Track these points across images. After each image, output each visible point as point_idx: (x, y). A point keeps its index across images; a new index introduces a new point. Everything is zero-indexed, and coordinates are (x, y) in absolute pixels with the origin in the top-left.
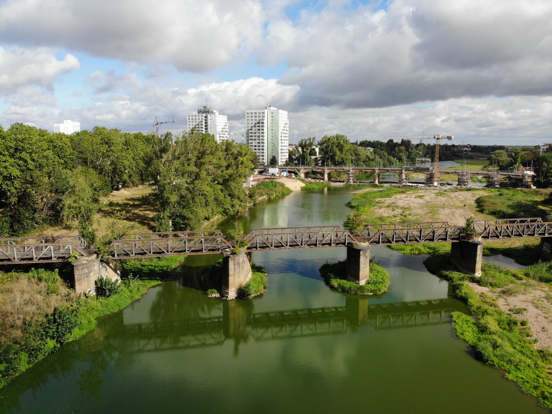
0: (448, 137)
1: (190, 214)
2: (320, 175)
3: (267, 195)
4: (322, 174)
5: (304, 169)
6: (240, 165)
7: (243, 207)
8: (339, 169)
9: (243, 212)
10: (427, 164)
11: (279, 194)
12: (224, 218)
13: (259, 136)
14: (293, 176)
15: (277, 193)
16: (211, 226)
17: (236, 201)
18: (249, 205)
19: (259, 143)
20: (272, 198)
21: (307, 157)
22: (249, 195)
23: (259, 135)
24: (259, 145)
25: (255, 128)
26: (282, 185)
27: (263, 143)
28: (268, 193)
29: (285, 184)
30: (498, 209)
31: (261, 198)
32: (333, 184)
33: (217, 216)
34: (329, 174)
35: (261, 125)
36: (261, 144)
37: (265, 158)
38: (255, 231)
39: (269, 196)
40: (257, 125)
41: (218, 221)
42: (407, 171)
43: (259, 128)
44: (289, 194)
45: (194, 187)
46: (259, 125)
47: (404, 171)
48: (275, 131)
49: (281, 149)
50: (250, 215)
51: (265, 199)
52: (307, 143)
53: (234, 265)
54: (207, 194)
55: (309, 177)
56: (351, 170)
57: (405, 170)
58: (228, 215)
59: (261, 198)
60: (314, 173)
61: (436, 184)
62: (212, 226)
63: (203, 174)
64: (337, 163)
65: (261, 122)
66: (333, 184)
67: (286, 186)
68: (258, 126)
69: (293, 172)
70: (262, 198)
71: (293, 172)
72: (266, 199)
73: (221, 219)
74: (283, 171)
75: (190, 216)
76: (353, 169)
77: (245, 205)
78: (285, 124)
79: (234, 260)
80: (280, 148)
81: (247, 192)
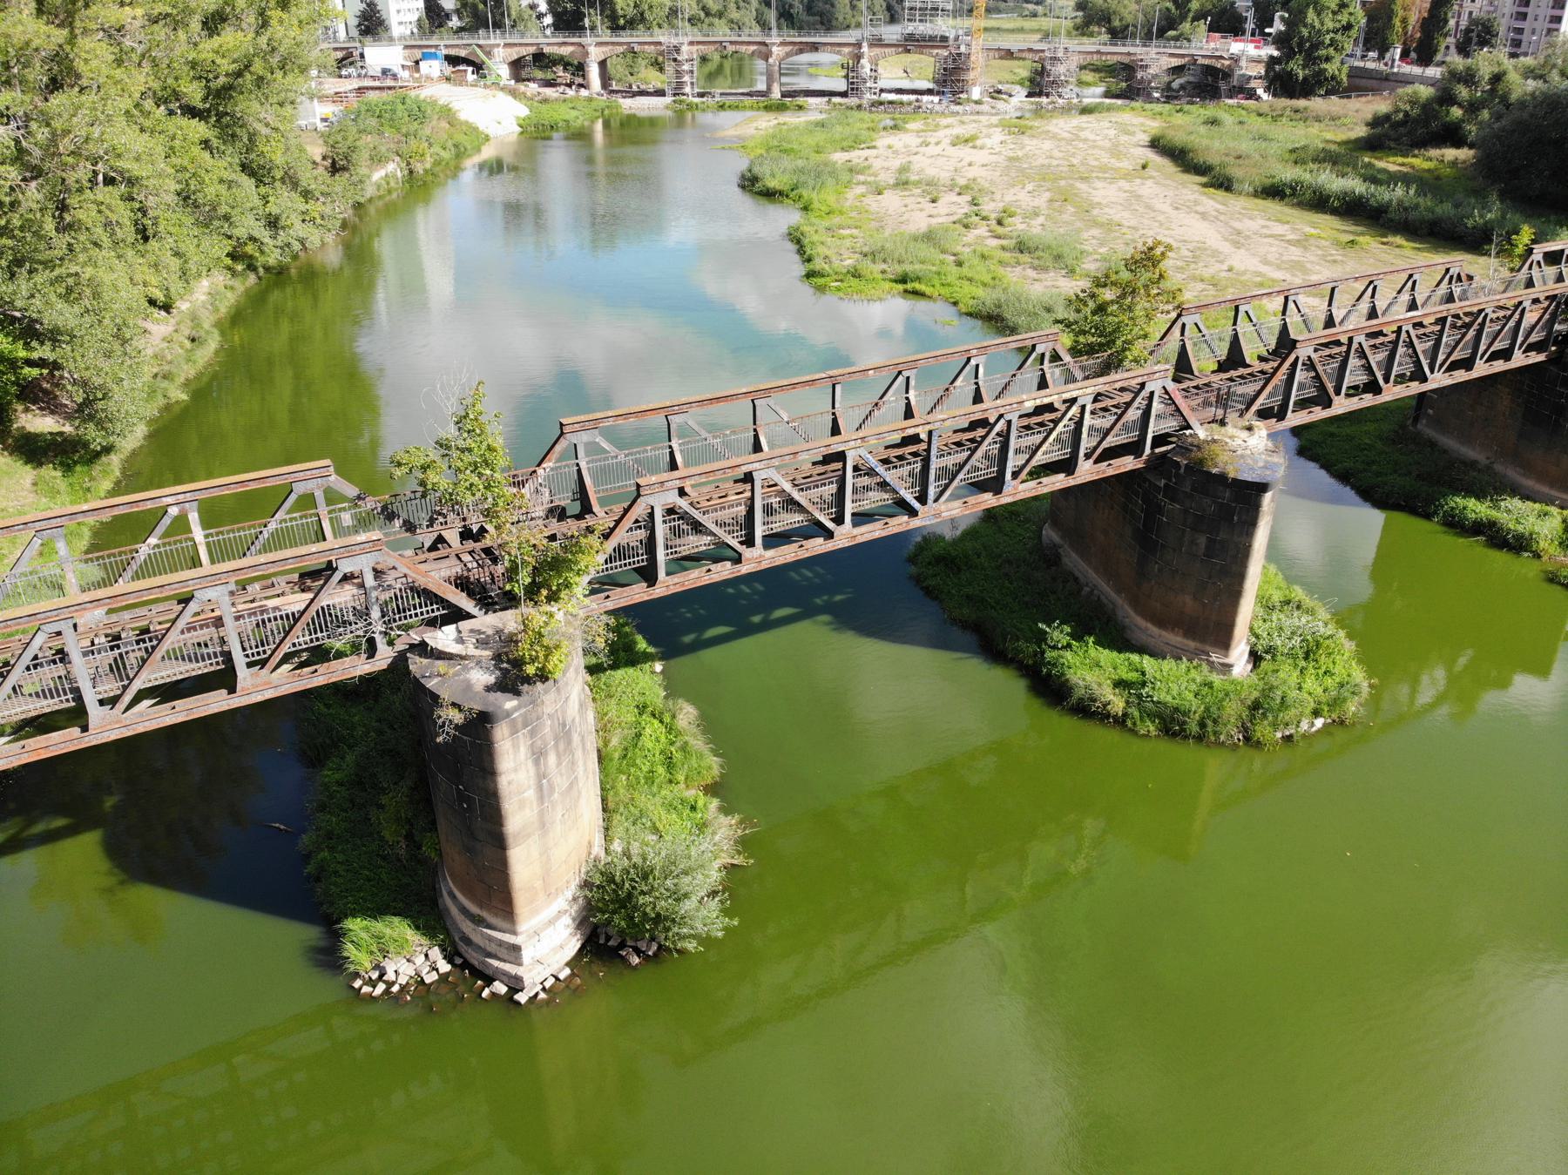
1: (60, 305)
2: (565, 69)
3: (397, 159)
5: (506, 45)
6: (279, 13)
7: (319, 221)
8: (639, 43)
10: (939, 21)
14: (471, 77)
15: (436, 149)
16: (188, 344)
17: (284, 201)
22: (328, 163)
26: (447, 114)
28: (404, 149)
29: (455, 106)
30: (1289, 179)
31: (377, 175)
32: (628, 105)
39: (408, 164)
41: (217, 310)
42: (876, 45)
45: (54, 134)
47: (865, 49)
53: (537, 762)
54: (136, 169)
55: (529, 80)
56: (685, 48)
57: (871, 45)
59: (377, 175)
60: (540, 59)
61: (976, 93)
63: (93, 55)
64: (622, 22)
66: (628, 105)
67: (462, 116)
70: (382, 173)
73: (229, 294)
74: (425, 57)
75: (58, 314)
76: (691, 43)
79: (531, 724)
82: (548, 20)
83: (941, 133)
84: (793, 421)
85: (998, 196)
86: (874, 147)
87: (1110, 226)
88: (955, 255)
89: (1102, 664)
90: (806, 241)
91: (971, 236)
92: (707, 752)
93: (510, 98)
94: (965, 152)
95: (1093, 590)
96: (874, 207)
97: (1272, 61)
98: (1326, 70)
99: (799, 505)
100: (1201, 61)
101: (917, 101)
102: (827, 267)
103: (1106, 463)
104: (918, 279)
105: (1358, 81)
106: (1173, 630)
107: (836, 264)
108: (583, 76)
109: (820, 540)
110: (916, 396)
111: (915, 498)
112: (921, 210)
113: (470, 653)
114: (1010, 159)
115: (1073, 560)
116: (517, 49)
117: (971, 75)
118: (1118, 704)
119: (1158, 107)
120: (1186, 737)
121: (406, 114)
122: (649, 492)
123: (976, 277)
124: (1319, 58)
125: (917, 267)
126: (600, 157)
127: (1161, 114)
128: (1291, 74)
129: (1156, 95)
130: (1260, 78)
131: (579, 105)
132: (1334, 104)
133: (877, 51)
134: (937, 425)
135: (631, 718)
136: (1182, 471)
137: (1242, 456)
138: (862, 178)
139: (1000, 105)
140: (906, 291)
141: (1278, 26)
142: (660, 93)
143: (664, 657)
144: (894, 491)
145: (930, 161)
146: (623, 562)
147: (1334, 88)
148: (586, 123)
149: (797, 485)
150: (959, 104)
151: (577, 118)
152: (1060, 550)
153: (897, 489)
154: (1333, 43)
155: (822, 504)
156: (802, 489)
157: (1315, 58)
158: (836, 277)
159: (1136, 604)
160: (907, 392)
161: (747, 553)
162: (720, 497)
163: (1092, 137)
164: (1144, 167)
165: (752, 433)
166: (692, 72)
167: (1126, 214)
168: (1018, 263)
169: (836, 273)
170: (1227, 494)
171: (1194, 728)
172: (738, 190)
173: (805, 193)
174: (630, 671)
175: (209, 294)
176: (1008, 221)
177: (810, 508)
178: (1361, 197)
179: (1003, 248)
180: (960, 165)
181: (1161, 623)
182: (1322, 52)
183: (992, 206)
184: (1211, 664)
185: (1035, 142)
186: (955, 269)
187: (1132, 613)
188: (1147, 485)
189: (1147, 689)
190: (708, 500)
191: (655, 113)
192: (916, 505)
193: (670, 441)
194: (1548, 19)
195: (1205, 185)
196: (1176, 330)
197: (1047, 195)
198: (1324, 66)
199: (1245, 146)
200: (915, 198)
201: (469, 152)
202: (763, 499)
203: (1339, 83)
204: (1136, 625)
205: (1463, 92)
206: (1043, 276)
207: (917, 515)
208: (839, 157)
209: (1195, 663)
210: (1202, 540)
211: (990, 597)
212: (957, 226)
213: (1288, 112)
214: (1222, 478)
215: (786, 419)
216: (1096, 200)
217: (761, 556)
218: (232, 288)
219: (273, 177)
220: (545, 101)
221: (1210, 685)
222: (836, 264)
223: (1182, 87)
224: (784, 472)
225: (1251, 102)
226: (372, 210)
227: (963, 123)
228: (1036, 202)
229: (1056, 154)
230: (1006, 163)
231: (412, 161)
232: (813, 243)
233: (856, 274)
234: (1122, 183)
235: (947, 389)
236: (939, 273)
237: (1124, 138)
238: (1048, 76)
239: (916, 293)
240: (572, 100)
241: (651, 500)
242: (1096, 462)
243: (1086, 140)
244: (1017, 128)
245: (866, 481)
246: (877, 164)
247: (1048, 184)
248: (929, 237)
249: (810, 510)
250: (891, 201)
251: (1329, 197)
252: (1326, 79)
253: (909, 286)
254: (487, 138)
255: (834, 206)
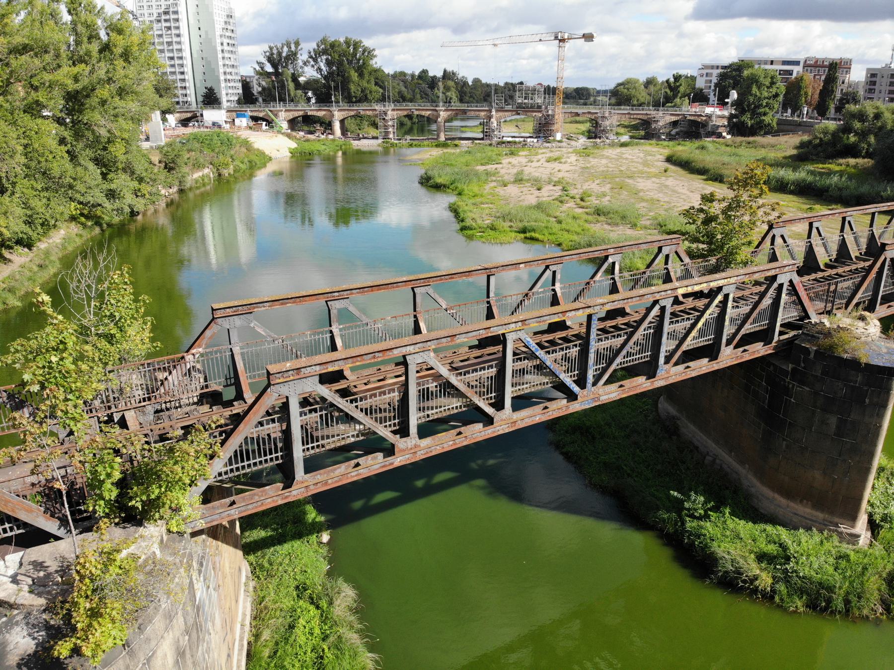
0: (584, 36)
2: (321, 125)
4: (328, 126)
5: (286, 111)
7: (147, 196)
9: (149, 213)
11: (241, 165)
12: (86, 234)
13: (169, 43)
14: (264, 127)
16: (35, 269)
18: (167, 192)
19: (172, 58)
20: (227, 175)
21: (288, 85)
23: (170, 40)
24: (172, 62)
25: (160, 24)
26: (246, 144)
27: (181, 58)
28: (216, 161)
31: (197, 175)
32: (356, 144)
33: (62, 232)
34: (342, 122)
35: (172, 16)
36: (177, 62)
37: (191, 91)
38: (238, 321)
39: (218, 170)
40: (163, 17)
43: (168, 24)
44: (264, 166)
46: (167, 17)
47: (494, 113)
48: (206, 32)
49: (225, 73)
50: (174, 219)
51: (208, 176)
52: (284, 54)
56: (390, 113)
57: (497, 111)
58: (100, 225)
59: (197, 175)
61: (558, 136)
62: (41, 266)
65: (171, 10)
66: (356, 144)
67: (256, 146)
68: (166, 21)
69: (263, 119)
70: (200, 174)
71: (263, 119)
72: (211, 175)
73: (77, 240)
77: (154, 190)
78: (228, 16)
80: (221, 70)
81: (155, 159)
82: (313, 101)
83: (540, 157)
84: (451, 308)
85: (579, 186)
86: (501, 163)
87: (652, 201)
88: (555, 218)
89: (742, 536)
90: (460, 210)
91: (565, 207)
92: (362, 649)
93: (286, 138)
94: (556, 166)
95: (714, 460)
96: (502, 193)
97: (731, 117)
98: (764, 120)
99: (457, 389)
100: (689, 118)
101: (524, 141)
102: (474, 224)
103: (741, 349)
104: (534, 230)
105: (782, 127)
106: (801, 502)
107: (479, 222)
108: (331, 129)
109: (479, 426)
110: (561, 289)
111: (574, 381)
112: (532, 194)
113: (20, 601)
114: (583, 168)
115: (690, 430)
116: (292, 113)
117: (554, 128)
118: (765, 580)
119: (666, 143)
120: (833, 613)
121: (219, 142)
122: (281, 380)
123: (572, 229)
124: (760, 114)
125: (533, 223)
126: (340, 171)
127: (668, 146)
128: (743, 123)
129: (663, 137)
130: (724, 126)
131: (327, 143)
132: (769, 139)
133: (501, 114)
134: (597, 309)
135: (287, 603)
136: (812, 356)
137: (866, 343)
138: (494, 178)
139: (573, 143)
140: (526, 238)
141: (734, 95)
142: (377, 138)
143: (331, 525)
144: (553, 374)
145: (535, 169)
146: (240, 465)
147: (768, 131)
148: (331, 153)
149: (456, 369)
150: (549, 142)
151: (326, 150)
152: (678, 422)
153: (557, 373)
154: (767, 105)
155: (480, 388)
156: (460, 374)
157: (757, 114)
158: (480, 230)
159: (761, 474)
160: (553, 284)
161: (401, 443)
162: (379, 381)
163: (630, 157)
164: (665, 171)
165: (413, 319)
166: (394, 126)
167: (661, 195)
168: (598, 221)
169: (480, 228)
170: (859, 379)
171: (839, 604)
172: (419, 186)
173: (459, 185)
174: (297, 544)
175: (64, 239)
176: (586, 199)
177: (469, 393)
178: (810, 183)
179: (587, 213)
180: (553, 171)
181: (789, 494)
182: (762, 110)
183: (576, 191)
184: (840, 534)
185: (596, 160)
186: (558, 226)
187: (755, 481)
188: (772, 368)
189: (792, 564)
190: (366, 384)
191: (372, 149)
192: (576, 389)
193: (331, 326)
194: (887, 92)
195: (706, 180)
196: (768, 240)
197: (609, 186)
198: (763, 118)
199: (726, 159)
200: (526, 188)
201: (258, 166)
202: (418, 384)
203: (772, 128)
204: (763, 496)
205: (857, 125)
206: (615, 228)
207: (576, 399)
208: (481, 168)
209: (825, 533)
210: (833, 421)
211: (625, 465)
212: (555, 201)
213: (744, 144)
214: (854, 364)
215: (444, 307)
216: (640, 188)
217: (416, 446)
218: (81, 236)
219: (117, 167)
220: (308, 140)
221: (846, 557)
222: (479, 222)
223: (677, 133)
224: (442, 356)
225: (721, 140)
226: (191, 195)
227: (552, 151)
228: (603, 189)
229: (610, 165)
230: (580, 170)
231: (220, 168)
232: (465, 211)
233: (493, 228)
234: (654, 179)
235: (588, 283)
236: (547, 227)
237: (649, 158)
238: (600, 127)
239: (532, 239)
240: (323, 140)
241: (284, 390)
242: (735, 348)
243: (627, 159)
244: (584, 153)
245: (526, 364)
246: (503, 172)
247: (608, 180)
248: (539, 207)
249: (469, 395)
250: (513, 190)
251: (787, 184)
252: (765, 125)
253: (528, 235)
254: (270, 159)
255: (478, 192)
